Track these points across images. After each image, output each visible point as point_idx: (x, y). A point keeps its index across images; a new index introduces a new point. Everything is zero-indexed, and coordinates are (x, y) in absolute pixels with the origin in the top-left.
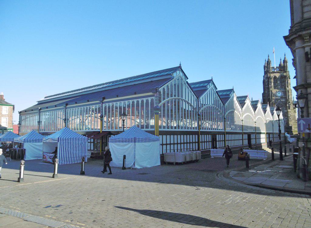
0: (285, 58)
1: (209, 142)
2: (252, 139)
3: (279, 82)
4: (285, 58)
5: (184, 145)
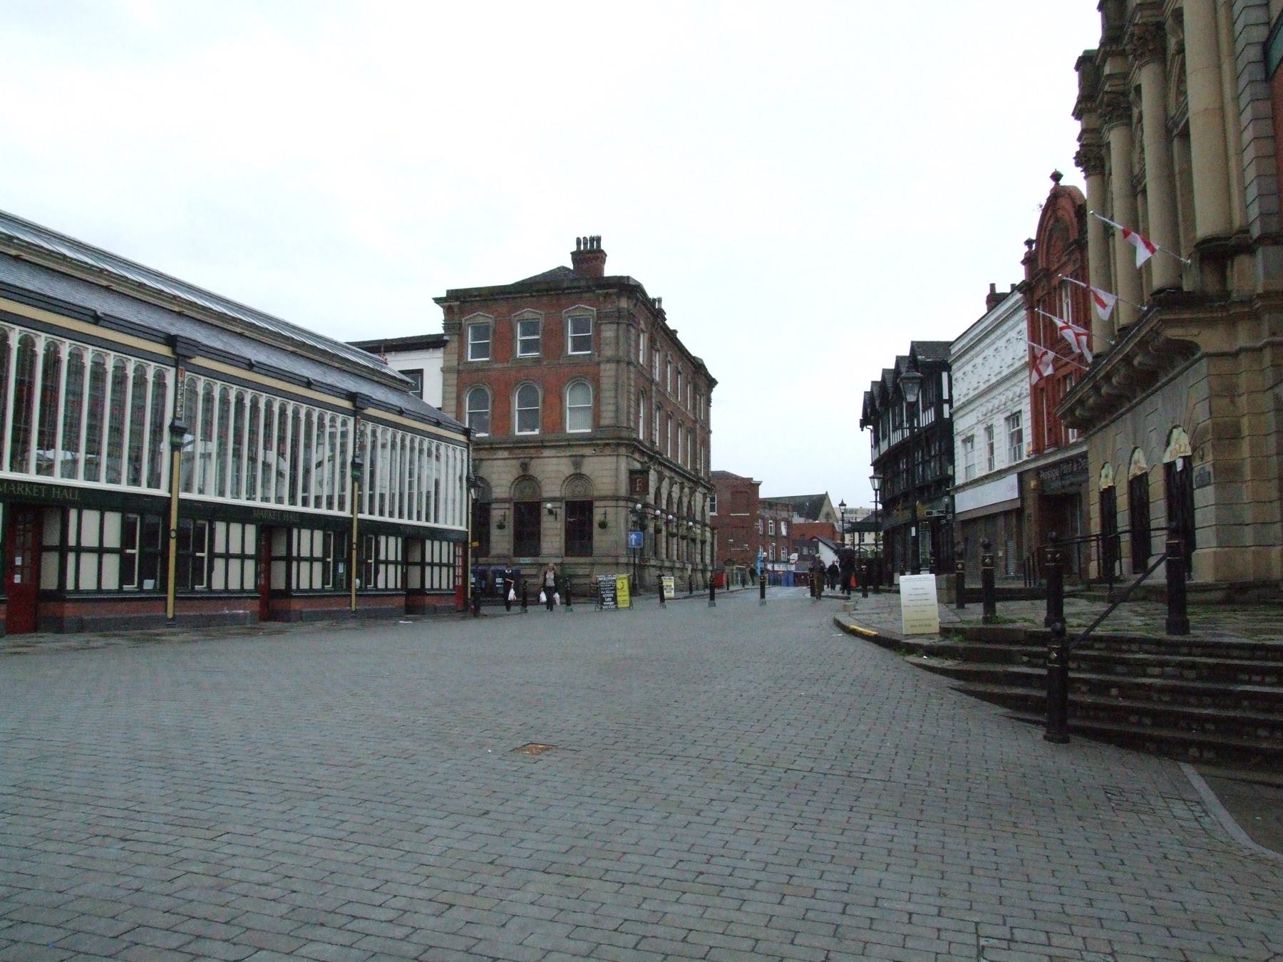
1: (243, 557)
2: (243, 557)
5: (441, 571)
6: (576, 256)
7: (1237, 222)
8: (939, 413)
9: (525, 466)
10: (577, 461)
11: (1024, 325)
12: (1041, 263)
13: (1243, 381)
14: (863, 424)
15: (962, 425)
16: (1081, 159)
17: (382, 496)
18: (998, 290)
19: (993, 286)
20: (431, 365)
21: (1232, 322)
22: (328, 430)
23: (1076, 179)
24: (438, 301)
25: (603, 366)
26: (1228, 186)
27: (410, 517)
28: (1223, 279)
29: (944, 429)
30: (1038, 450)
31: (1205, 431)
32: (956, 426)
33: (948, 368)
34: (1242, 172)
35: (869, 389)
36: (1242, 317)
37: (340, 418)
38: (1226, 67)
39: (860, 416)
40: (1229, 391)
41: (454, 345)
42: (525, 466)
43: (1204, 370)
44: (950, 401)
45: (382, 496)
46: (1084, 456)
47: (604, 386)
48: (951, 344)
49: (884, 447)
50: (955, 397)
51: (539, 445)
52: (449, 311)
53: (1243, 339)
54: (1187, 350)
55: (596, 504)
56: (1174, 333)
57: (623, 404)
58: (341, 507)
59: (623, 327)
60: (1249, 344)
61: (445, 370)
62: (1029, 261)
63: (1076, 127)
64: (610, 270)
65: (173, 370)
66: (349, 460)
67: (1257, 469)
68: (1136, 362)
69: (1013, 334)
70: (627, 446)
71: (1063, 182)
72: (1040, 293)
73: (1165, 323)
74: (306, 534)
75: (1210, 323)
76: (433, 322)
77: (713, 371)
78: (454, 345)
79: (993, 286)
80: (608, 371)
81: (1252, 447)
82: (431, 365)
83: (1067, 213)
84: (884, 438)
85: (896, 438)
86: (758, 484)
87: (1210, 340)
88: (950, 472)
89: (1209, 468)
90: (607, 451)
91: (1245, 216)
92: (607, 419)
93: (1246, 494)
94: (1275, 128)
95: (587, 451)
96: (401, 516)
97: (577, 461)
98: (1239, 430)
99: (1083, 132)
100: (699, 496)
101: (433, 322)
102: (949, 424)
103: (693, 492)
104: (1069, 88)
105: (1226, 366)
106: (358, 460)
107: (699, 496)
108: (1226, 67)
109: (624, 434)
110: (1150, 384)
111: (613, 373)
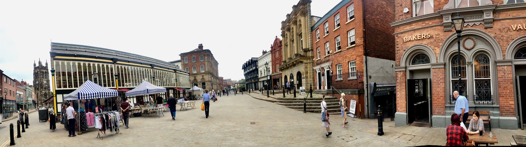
0: (47, 62)
3: (44, 75)
4: (47, 62)
6: (199, 47)
7: (308, 47)
8: (256, 67)
9: (195, 78)
10: (203, 76)
11: (271, 56)
12: (274, 48)
13: (308, 66)
14: (242, 69)
15: (260, 69)
16: (282, 35)
17: (173, 84)
18: (264, 51)
19: (263, 50)
20: (180, 64)
21: (307, 59)
22: (167, 75)
23: (281, 38)
24: (179, 55)
25: (205, 63)
26: (307, 43)
27: (167, 86)
28: (306, 54)
29: (257, 70)
30: (273, 73)
31: (304, 72)
32: (259, 69)
33: (257, 61)
34: (308, 41)
35: (244, 64)
36: (309, 59)
37: (149, 69)
38: (307, 29)
39: (242, 68)
40: (306, 68)
41: (183, 61)
42: (195, 78)
43: (304, 65)
44: (258, 66)
45: (173, 84)
46: (282, 73)
47: (206, 65)
48: (258, 58)
49: (246, 72)
50: (258, 65)
51: (197, 74)
52: (181, 56)
53: (308, 61)
54: (302, 62)
55: (206, 82)
56: (301, 60)
57: (209, 68)
58: (175, 86)
59: (208, 57)
60: (309, 62)
61: (181, 65)
62: (272, 47)
63: (281, 31)
64: (204, 49)
65: (152, 69)
66: (152, 76)
67: (310, 77)
68: (294, 63)
69: (269, 57)
70: (210, 73)
71: (277, 37)
72: (273, 52)
73: (300, 59)
74: (171, 90)
75: (305, 59)
76: (179, 58)
77: (218, 62)
78: (183, 61)
79: (263, 50)
80: (206, 63)
81: (309, 74)
82: (180, 64)
83: (278, 42)
84: (246, 71)
85: (248, 71)
86: (223, 78)
87: (305, 61)
88: (258, 75)
89: (305, 77)
90: (207, 74)
91: (309, 47)
92: (207, 70)
93: (309, 80)
94: (312, 35)
95: (204, 75)
96: (173, 86)
97: (203, 76)
98: (308, 72)
99: (282, 32)
100: (218, 80)
101: (179, 58)
102: (258, 69)
103: (217, 79)
104: (280, 26)
105: (307, 64)
106: (154, 77)
107: (218, 80)
108: (307, 29)
109: (209, 72)
110: (294, 66)
111: (207, 63)
